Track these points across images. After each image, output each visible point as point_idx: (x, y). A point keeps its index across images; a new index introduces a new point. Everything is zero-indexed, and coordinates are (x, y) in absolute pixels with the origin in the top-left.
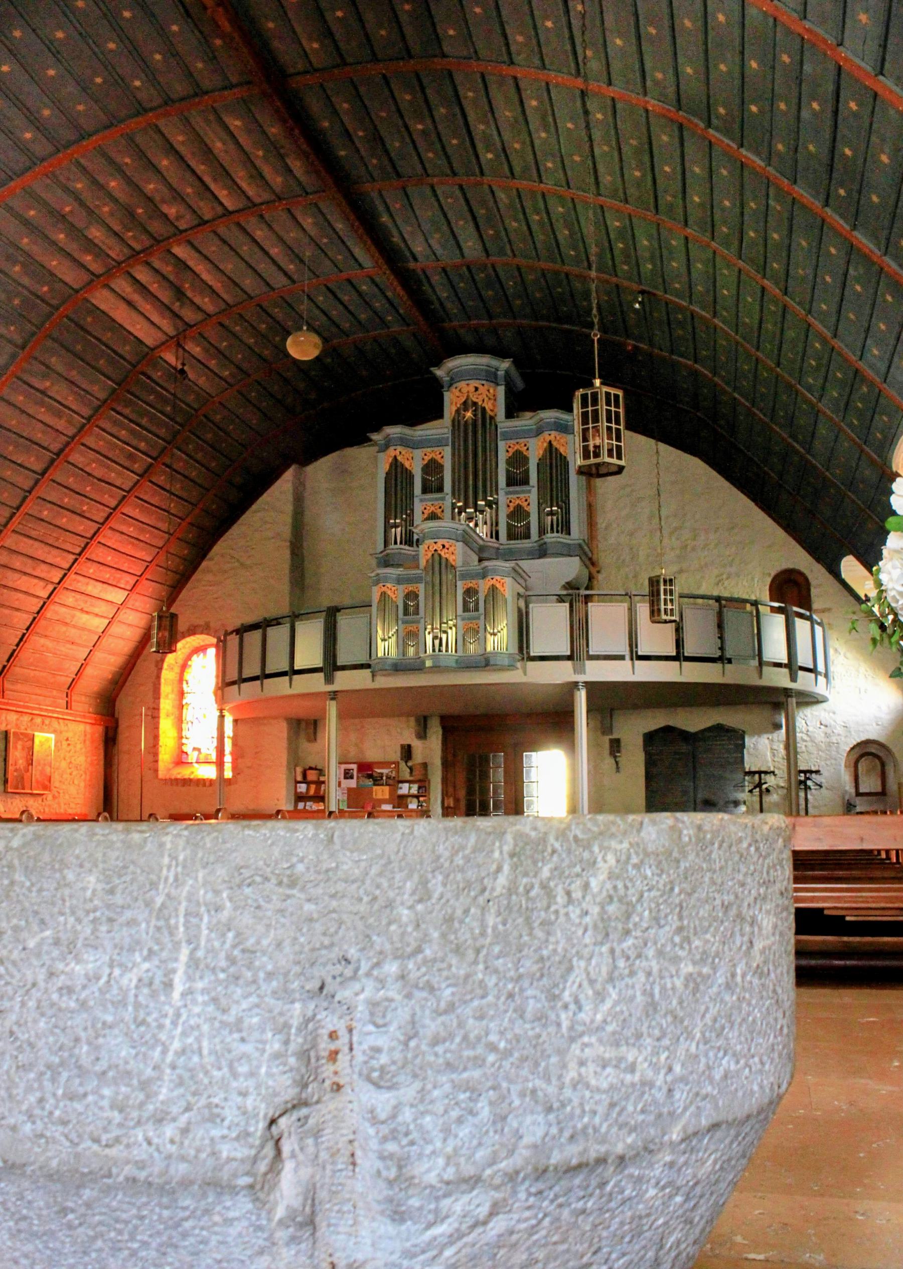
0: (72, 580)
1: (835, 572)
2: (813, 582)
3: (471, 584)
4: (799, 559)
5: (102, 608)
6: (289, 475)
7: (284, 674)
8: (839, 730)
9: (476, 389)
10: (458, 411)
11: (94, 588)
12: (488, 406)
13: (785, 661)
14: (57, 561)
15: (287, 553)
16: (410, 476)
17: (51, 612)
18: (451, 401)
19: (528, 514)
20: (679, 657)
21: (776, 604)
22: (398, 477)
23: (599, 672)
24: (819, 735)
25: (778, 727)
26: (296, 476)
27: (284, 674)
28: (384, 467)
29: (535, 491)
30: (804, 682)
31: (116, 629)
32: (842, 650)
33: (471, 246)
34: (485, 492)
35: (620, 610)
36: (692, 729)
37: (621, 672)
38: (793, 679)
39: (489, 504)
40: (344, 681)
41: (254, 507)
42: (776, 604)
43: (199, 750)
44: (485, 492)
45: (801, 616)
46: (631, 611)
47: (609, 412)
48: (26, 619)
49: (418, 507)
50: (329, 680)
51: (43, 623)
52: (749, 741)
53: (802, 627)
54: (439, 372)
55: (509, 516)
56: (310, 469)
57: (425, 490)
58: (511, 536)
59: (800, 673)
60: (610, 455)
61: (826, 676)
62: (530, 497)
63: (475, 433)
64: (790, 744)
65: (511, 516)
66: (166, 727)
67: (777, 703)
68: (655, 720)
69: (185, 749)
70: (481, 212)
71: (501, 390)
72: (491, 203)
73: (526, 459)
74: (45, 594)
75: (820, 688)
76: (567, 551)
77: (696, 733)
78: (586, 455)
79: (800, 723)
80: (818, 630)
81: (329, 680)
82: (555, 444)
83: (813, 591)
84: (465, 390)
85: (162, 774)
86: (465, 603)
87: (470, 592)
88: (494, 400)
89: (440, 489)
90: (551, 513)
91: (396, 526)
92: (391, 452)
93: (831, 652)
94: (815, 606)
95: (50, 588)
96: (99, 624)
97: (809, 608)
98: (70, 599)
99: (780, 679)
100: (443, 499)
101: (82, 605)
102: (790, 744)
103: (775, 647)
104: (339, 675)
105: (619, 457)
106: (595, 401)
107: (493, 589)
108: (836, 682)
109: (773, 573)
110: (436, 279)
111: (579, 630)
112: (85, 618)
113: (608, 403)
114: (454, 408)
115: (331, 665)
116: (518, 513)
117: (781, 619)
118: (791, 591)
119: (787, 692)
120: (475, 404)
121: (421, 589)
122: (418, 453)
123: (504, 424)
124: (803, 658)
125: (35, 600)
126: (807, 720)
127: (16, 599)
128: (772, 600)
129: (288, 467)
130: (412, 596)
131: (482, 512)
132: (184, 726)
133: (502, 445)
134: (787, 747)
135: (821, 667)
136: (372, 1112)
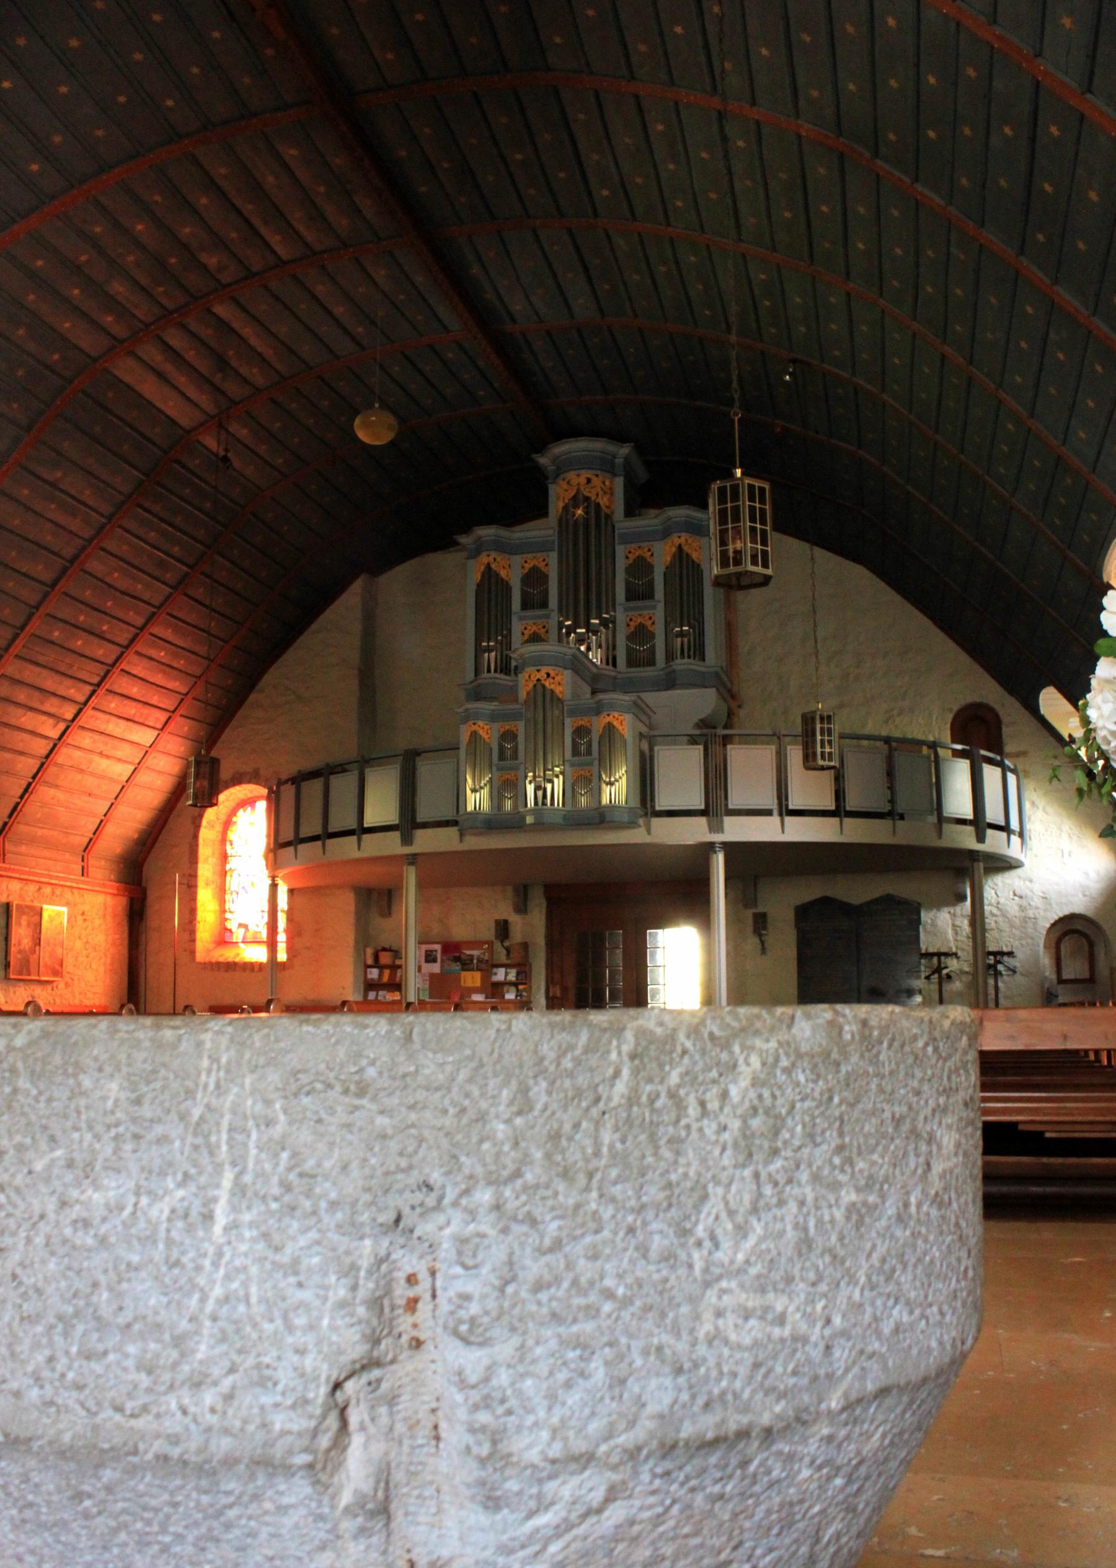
0: (90, 717)
2: (1005, 719)
5: (125, 751)
6: (357, 586)
8: (1037, 902)
9: (589, 481)
10: (566, 508)
11: (116, 727)
12: (603, 501)
13: (971, 817)
14: (72, 693)
15: (354, 684)
17: (63, 756)
18: (558, 495)
19: (652, 636)
20: (839, 812)
21: (959, 747)
22: (492, 589)
24: (1012, 908)
28: (475, 575)
30: (994, 842)
31: (143, 777)
32: (1041, 802)
35: (766, 754)
38: (981, 838)
39: (605, 623)
41: (314, 626)
42: (959, 747)
43: (246, 927)
45: (990, 761)
47: (752, 509)
49: (517, 627)
50: (407, 840)
53: (991, 775)
54: (543, 460)
56: (383, 579)
57: (525, 606)
58: (631, 662)
59: (990, 832)
61: (1021, 835)
62: (656, 615)
63: (587, 536)
65: (631, 638)
66: (205, 897)
69: (229, 925)
71: (619, 483)
73: (650, 568)
74: (54, 734)
75: (1014, 849)
76: (700, 681)
79: (989, 894)
80: (1012, 779)
81: (407, 840)
83: (1005, 730)
84: (575, 481)
88: (610, 494)
89: (544, 604)
90: (681, 634)
91: (489, 650)
92: (484, 559)
93: (1027, 806)
94: (1008, 748)
95: (62, 726)
96: (122, 771)
97: (999, 750)
98: (86, 740)
99: (966, 839)
100: (548, 617)
101: (101, 747)
102: (977, 918)
103: (958, 799)
105: (765, 565)
106: (735, 496)
109: (955, 708)
111: (716, 780)
112: (104, 763)
113: (752, 499)
114: (561, 505)
115: (409, 823)
116: (641, 634)
121: (521, 727)
122: (517, 560)
123: (623, 524)
124: (993, 812)
125: (43, 742)
126: (998, 890)
127: (20, 740)
129: (355, 577)
130: (509, 736)
131: (595, 633)
133: (620, 550)
135: (1014, 824)
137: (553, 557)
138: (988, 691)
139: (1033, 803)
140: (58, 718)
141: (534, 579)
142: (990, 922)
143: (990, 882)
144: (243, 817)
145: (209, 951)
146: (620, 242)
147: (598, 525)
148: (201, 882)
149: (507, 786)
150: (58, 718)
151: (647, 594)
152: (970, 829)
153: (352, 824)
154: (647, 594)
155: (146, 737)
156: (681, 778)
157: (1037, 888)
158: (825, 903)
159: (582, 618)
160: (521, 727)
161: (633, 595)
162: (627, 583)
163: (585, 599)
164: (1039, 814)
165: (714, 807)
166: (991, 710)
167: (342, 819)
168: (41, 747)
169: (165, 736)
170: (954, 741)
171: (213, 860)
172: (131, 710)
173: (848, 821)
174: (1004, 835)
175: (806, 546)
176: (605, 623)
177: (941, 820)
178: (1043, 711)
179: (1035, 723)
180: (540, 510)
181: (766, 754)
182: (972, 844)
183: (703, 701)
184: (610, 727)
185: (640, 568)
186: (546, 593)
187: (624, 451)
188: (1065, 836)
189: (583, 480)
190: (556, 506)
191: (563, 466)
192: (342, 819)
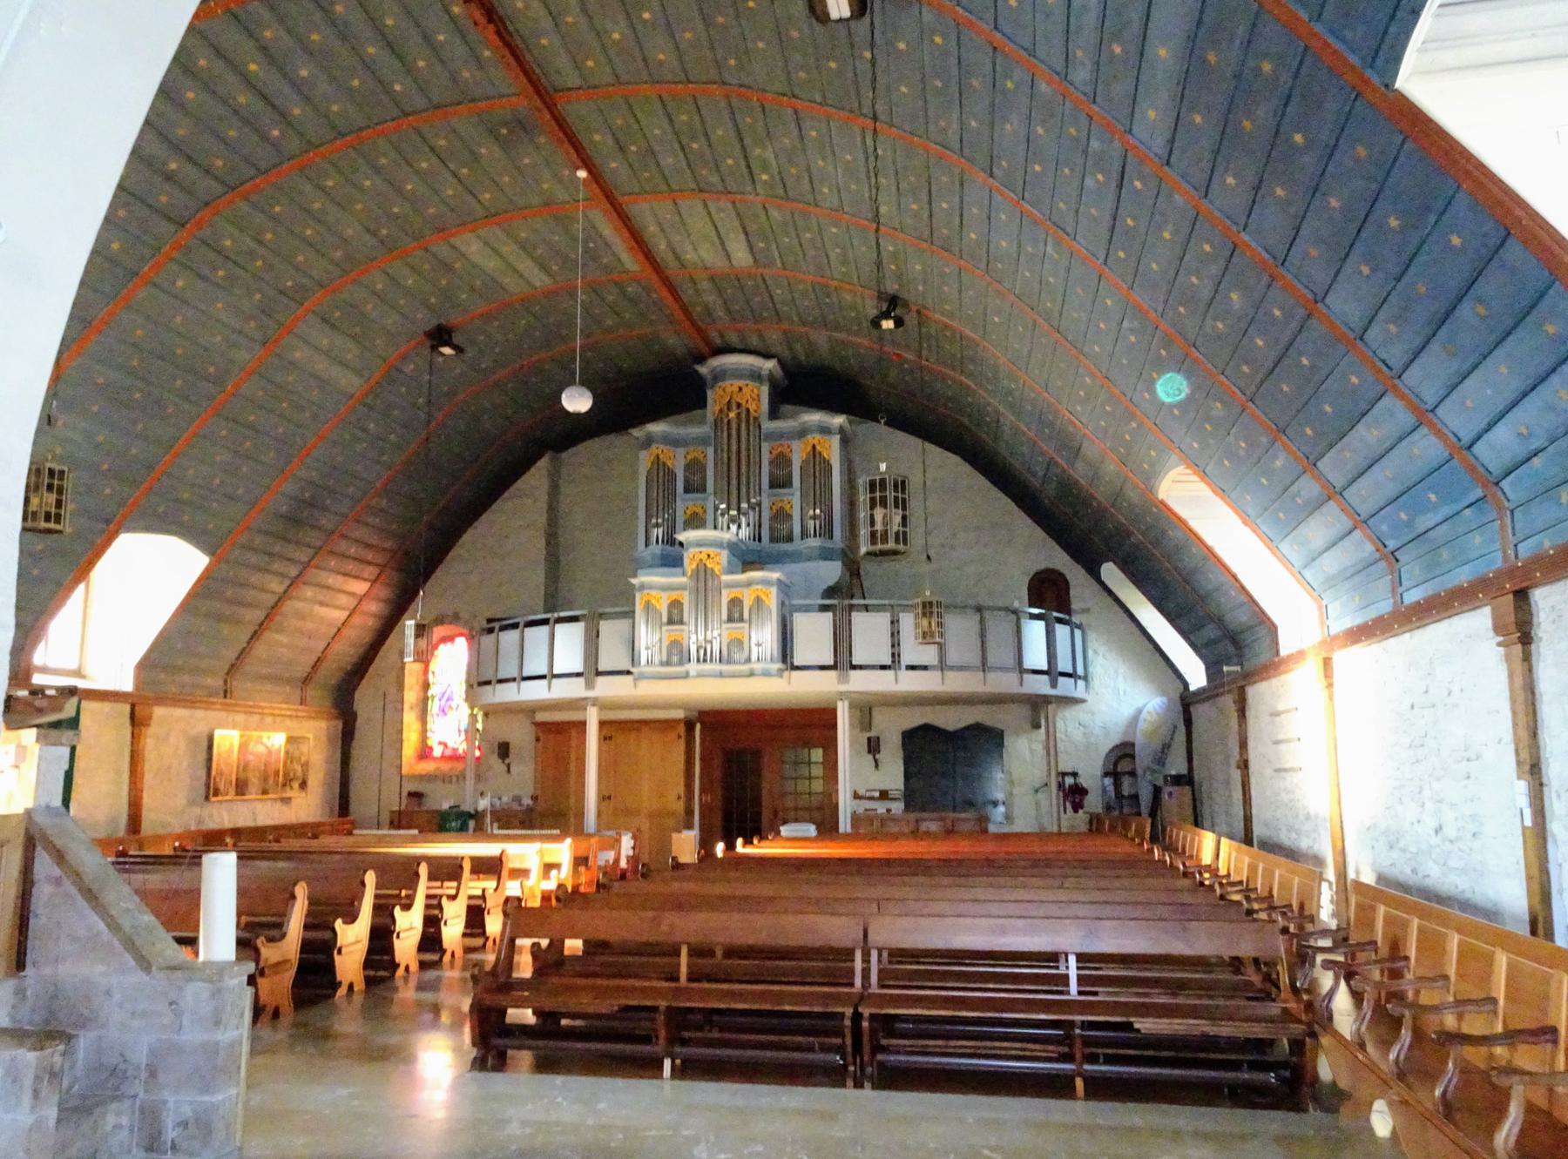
0: (312, 574)
2: (1072, 583)
3: (735, 593)
5: (343, 600)
6: (543, 463)
7: (543, 677)
8: (1097, 731)
10: (721, 411)
16: (671, 475)
17: (290, 606)
18: (715, 399)
19: (790, 516)
20: (943, 666)
21: (1036, 611)
22: (661, 476)
24: (1078, 735)
25: (1037, 726)
26: (552, 459)
28: (645, 460)
30: (1065, 686)
32: (1102, 650)
35: (883, 619)
36: (951, 727)
38: (1054, 685)
39: (751, 507)
41: (506, 495)
42: (1036, 611)
43: (446, 745)
45: (1060, 621)
47: (896, 498)
48: (259, 615)
49: (680, 506)
51: (277, 618)
53: (1062, 631)
56: (564, 455)
57: (687, 490)
59: (1061, 679)
60: (897, 541)
61: (1085, 678)
62: (793, 499)
63: (737, 433)
64: (1051, 748)
66: (410, 718)
70: (752, 227)
71: (765, 389)
73: (789, 463)
74: (281, 589)
75: (1079, 690)
76: (826, 555)
77: (956, 732)
79: (1060, 725)
80: (1078, 633)
81: (590, 685)
82: (818, 448)
83: (1072, 592)
84: (729, 390)
86: (729, 611)
87: (735, 603)
88: (759, 398)
89: (703, 489)
90: (814, 517)
91: (657, 525)
93: (1090, 653)
94: (1075, 606)
95: (287, 582)
96: (341, 615)
97: (1068, 612)
98: (309, 592)
99: (1041, 686)
100: (705, 499)
101: (320, 597)
102: (1051, 748)
103: (1036, 656)
107: (758, 600)
108: (1096, 683)
110: (705, 285)
113: (896, 490)
114: (717, 408)
115: (592, 670)
116: (781, 516)
117: (1040, 626)
118: (1049, 594)
119: (1046, 700)
120: (739, 405)
121: (686, 598)
122: (681, 451)
123: (768, 425)
124: (1064, 664)
126: (1067, 723)
127: (250, 595)
128: (1031, 605)
130: (676, 605)
133: (765, 447)
135: (1080, 671)
137: (710, 451)
138: (1060, 560)
139: (1095, 652)
140: (283, 575)
144: (443, 650)
147: (748, 421)
149: (730, 846)
151: (785, 483)
152: (1045, 678)
153: (543, 671)
154: (785, 483)
155: (361, 587)
157: (1099, 721)
158: (927, 729)
160: (686, 598)
161: (775, 484)
162: (771, 474)
163: (737, 489)
165: (842, 661)
167: (536, 665)
168: (270, 599)
169: (377, 586)
172: (350, 566)
174: (1072, 680)
175: (919, 441)
176: (751, 507)
177: (1022, 671)
178: (1103, 577)
179: (1096, 586)
180: (702, 403)
181: (883, 619)
183: (832, 571)
185: (781, 461)
186: (704, 478)
188: (1121, 679)
190: (712, 408)
191: (719, 375)
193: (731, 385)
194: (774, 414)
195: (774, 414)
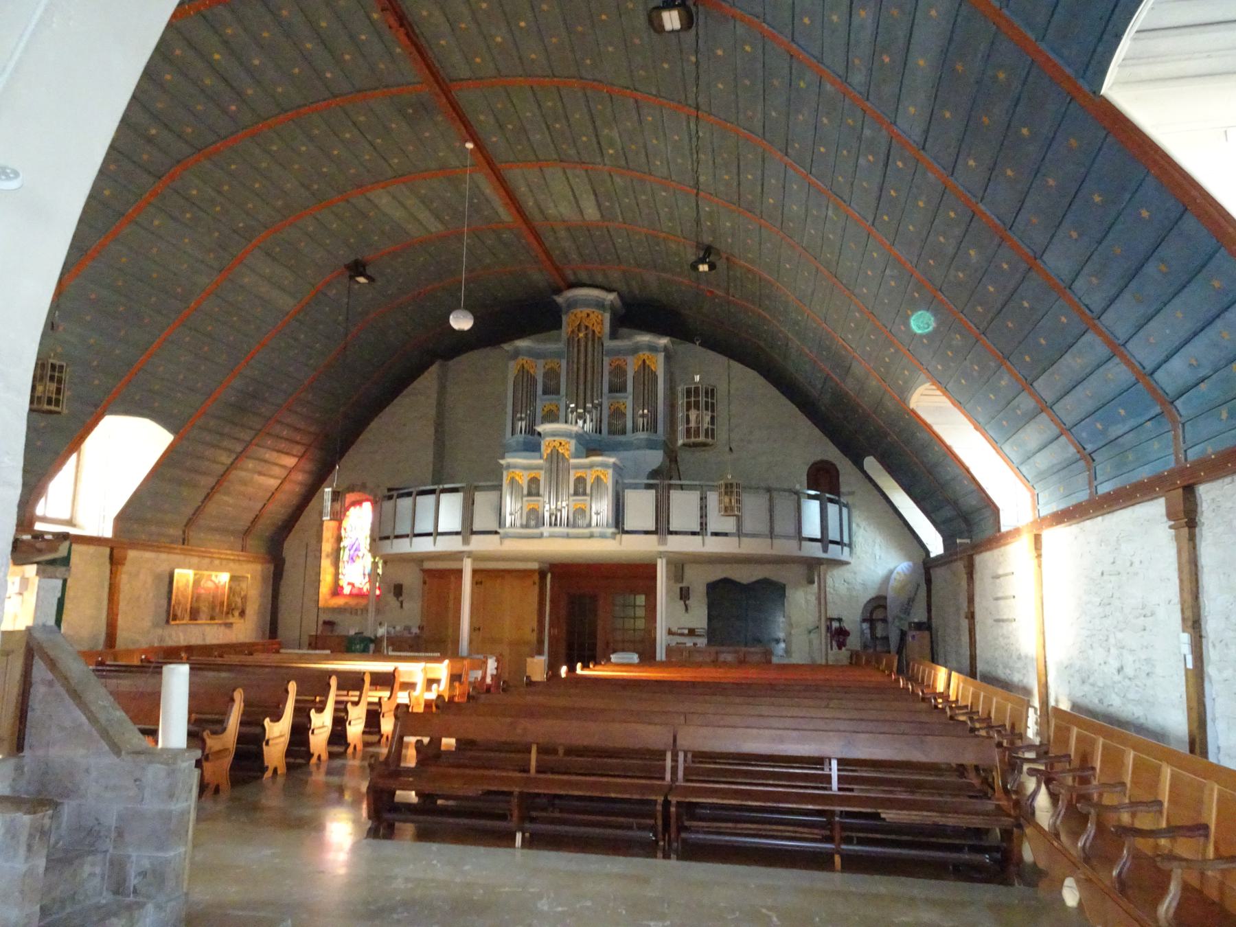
0: (253, 449)
1: (859, 464)
2: (841, 472)
4: (832, 453)
6: (434, 369)
7: (429, 534)
10: (573, 332)
11: (269, 455)
12: (597, 329)
13: (819, 536)
14: (242, 435)
16: (533, 380)
18: (568, 322)
19: (624, 415)
20: (739, 533)
21: (812, 492)
22: (525, 380)
23: (676, 544)
24: (842, 589)
27: (429, 534)
28: (513, 368)
29: (631, 397)
30: (834, 552)
31: (287, 487)
32: (863, 524)
33: (591, 212)
34: (592, 396)
35: (694, 496)
36: (745, 581)
37: (691, 545)
38: (825, 550)
39: (595, 407)
40: (479, 544)
42: (812, 492)
43: (353, 585)
44: (592, 396)
45: (831, 501)
46: (703, 499)
47: (707, 403)
50: (466, 541)
52: (789, 592)
53: (832, 509)
54: (559, 299)
55: (609, 416)
56: (451, 363)
57: (545, 392)
58: (610, 432)
59: (831, 546)
60: (707, 436)
61: (850, 545)
62: (627, 401)
65: (611, 416)
67: (813, 569)
68: (718, 573)
71: (607, 316)
72: (609, 183)
73: (624, 373)
74: (228, 461)
75: (845, 555)
76: (651, 445)
78: (688, 436)
79: (829, 581)
80: (845, 510)
81: (466, 541)
84: (579, 315)
85: (321, 604)
87: (580, 481)
89: (557, 392)
90: (643, 416)
91: (521, 419)
93: (854, 526)
94: (843, 489)
95: (234, 456)
96: (274, 483)
97: (838, 493)
98: (250, 464)
99: (815, 550)
101: (259, 468)
102: (822, 599)
103: (812, 527)
104: (474, 538)
110: (563, 234)
111: (662, 511)
113: (707, 396)
116: (618, 414)
118: (824, 480)
120: (587, 327)
121: (542, 476)
122: (541, 362)
124: (833, 534)
126: (836, 581)
129: (432, 363)
130: (534, 481)
132: (341, 564)
134: (819, 599)
135: (846, 540)
136: (21, 594)
137: (564, 363)
139: (858, 525)
140: (230, 451)
141: (552, 375)
142: (829, 597)
143: (829, 574)
145: (326, 601)
146: (618, 180)
148: (323, 555)
150: (230, 451)
153: (430, 529)
155: (290, 461)
156: (641, 507)
158: (726, 581)
159: (581, 402)
160: (542, 476)
164: (861, 531)
165: (662, 528)
166: (833, 465)
167: (425, 525)
170: (809, 488)
171: (332, 540)
173: (744, 540)
177: (801, 539)
178: (866, 468)
179: (860, 475)
181: (694, 496)
182: (821, 554)
184: (598, 479)
185: (619, 372)
187: (611, 297)
189: (584, 315)
190: (566, 330)
192: (425, 525)
193: (581, 312)
194: (614, 335)
195: (614, 335)
